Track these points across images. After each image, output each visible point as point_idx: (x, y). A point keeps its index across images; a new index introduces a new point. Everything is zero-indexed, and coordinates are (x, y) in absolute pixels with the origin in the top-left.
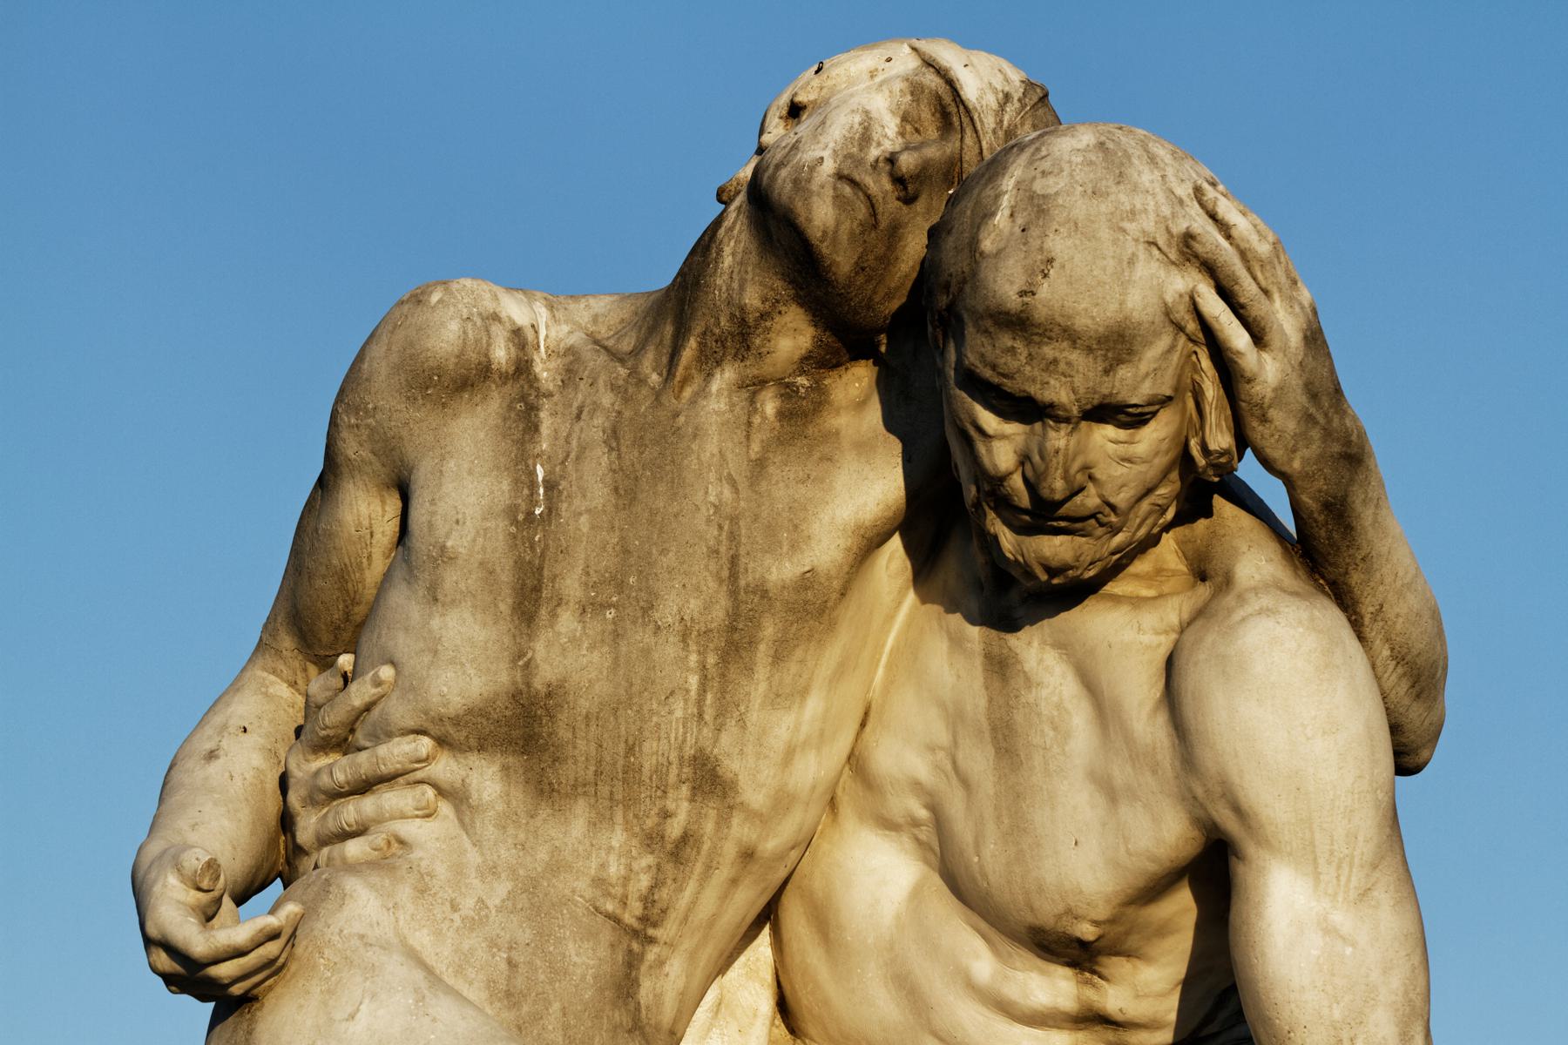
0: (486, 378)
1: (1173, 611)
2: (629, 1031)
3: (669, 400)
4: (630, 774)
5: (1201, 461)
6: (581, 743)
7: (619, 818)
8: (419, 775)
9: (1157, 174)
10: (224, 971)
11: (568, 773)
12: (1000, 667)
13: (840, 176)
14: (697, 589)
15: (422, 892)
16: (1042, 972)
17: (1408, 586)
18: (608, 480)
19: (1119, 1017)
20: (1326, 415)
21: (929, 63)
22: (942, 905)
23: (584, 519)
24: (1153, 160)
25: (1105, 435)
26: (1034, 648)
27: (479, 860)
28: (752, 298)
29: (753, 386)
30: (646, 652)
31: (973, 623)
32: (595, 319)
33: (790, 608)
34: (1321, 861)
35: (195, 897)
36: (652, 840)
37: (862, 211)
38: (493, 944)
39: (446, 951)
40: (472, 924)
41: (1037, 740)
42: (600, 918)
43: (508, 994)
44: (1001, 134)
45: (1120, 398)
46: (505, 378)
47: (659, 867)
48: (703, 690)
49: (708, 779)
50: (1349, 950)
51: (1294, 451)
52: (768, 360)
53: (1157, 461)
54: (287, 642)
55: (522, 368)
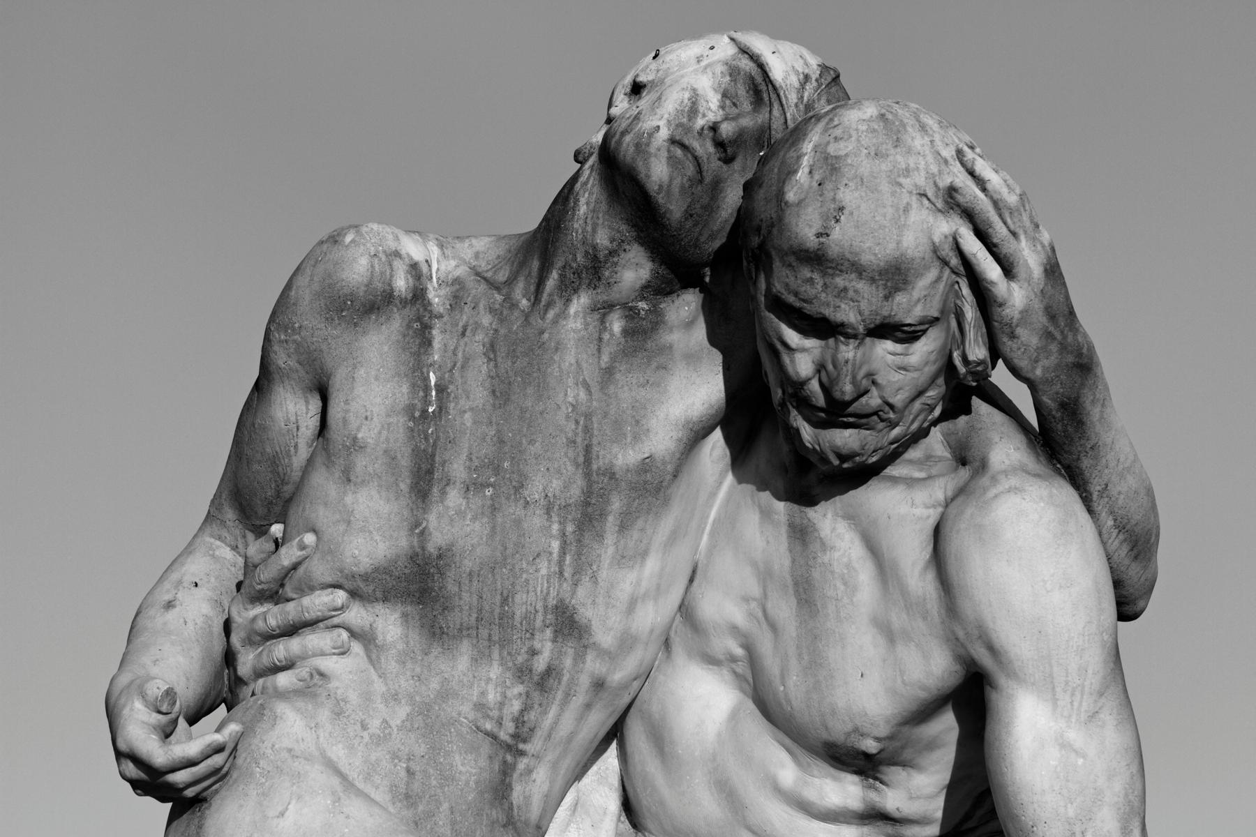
0: (389, 302)
1: (939, 490)
2: (504, 826)
3: (536, 321)
4: (505, 619)
5: (962, 370)
6: (465, 595)
7: (496, 655)
8: (336, 621)
9: (927, 139)
10: (180, 777)
11: (455, 619)
12: (801, 535)
13: (673, 141)
14: (559, 472)
15: (338, 714)
16: (835, 779)
17: (1128, 469)
18: (487, 385)
19: (896, 815)
20: (1062, 332)
21: (744, 51)
23: (467, 416)
24: (923, 128)
25: (885, 349)
26: (828, 519)
27: (384, 689)
28: (602, 239)
29: (603, 309)
30: (518, 522)
31: (779, 499)
32: (477, 255)
34: (1058, 690)
35: (156, 718)
36: (522, 673)
37: (690, 169)
38: (395, 756)
39: (358, 762)
40: (380, 740)
41: (830, 593)
42: (481, 735)
44: (802, 107)
45: (897, 319)
46: (404, 303)
47: (528, 695)
48: (563, 552)
49: (568, 624)
50: (1080, 761)
52: (615, 288)
53: (927, 369)
54: (230, 514)
55: (418, 295)
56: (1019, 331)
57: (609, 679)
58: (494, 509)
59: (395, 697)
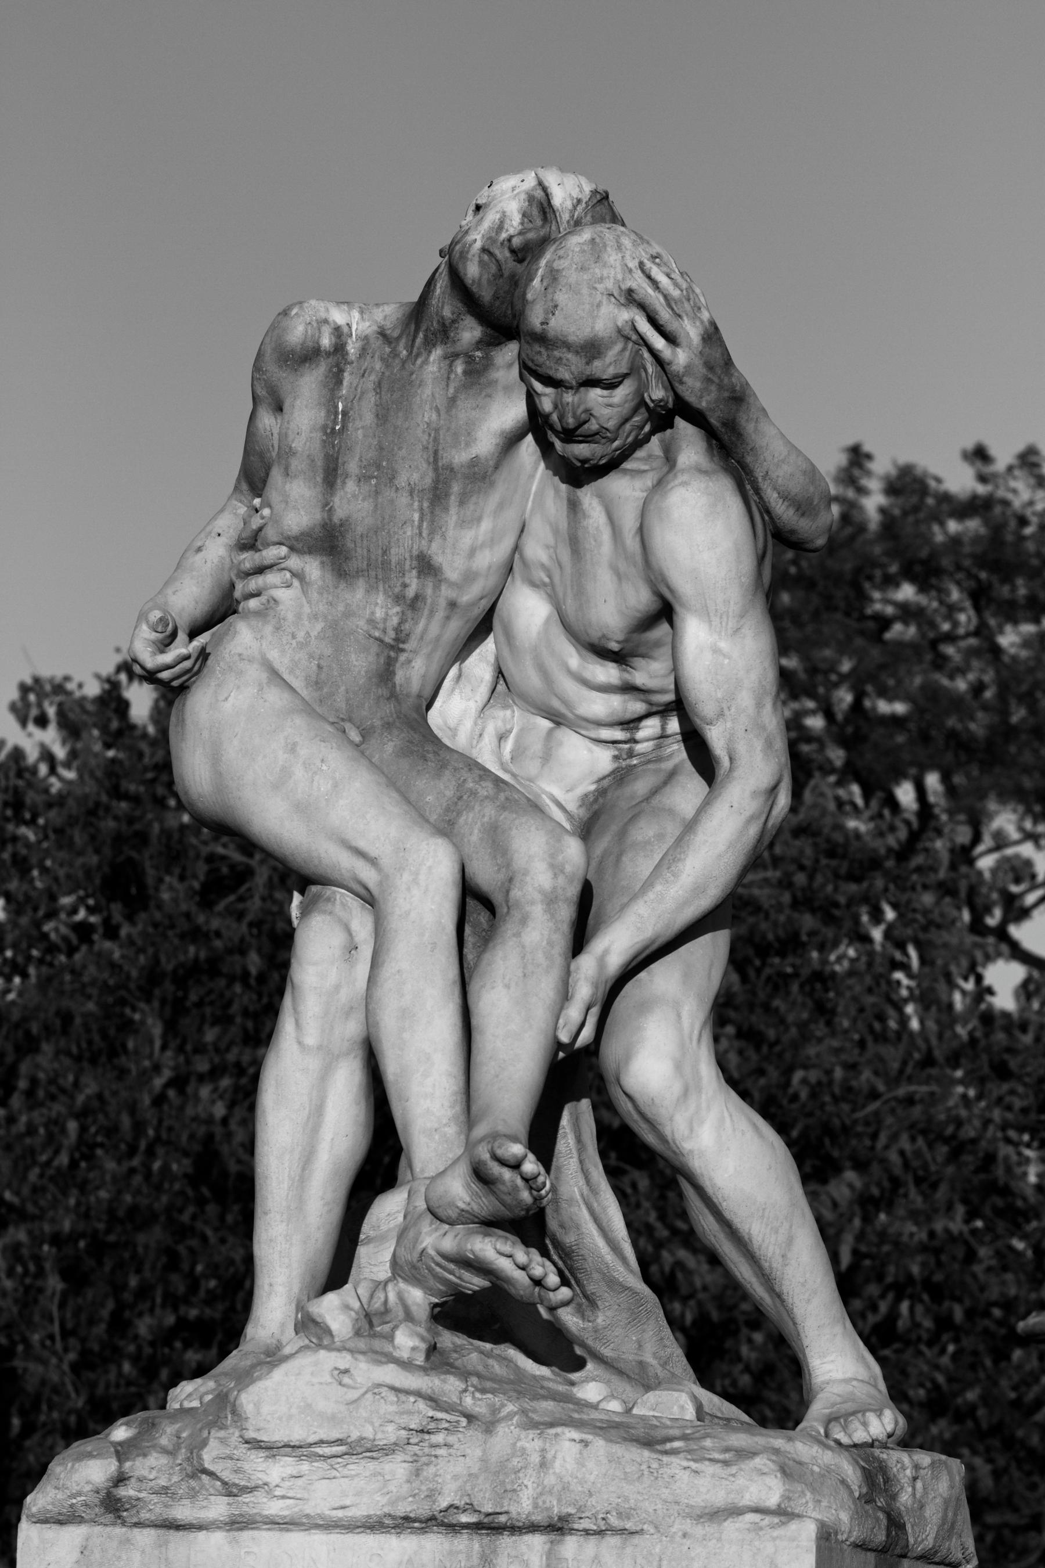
0: (318, 355)
1: (649, 481)
2: (388, 699)
3: (409, 366)
4: (386, 565)
5: (652, 405)
7: (381, 588)
8: (283, 566)
9: (620, 255)
10: (165, 675)
11: (353, 565)
12: (574, 506)
13: (484, 250)
14: (417, 467)
15: (278, 629)
16: (602, 665)
17: (783, 461)
19: (643, 688)
20: (719, 377)
21: (540, 184)
22: (557, 630)
23: (360, 432)
24: (619, 247)
25: (595, 395)
26: (587, 496)
27: (309, 611)
28: (447, 312)
29: (451, 358)
30: (392, 502)
31: (563, 482)
32: (385, 317)
33: (466, 477)
35: (154, 636)
36: (399, 599)
37: (493, 268)
38: (311, 656)
39: (286, 661)
40: (302, 646)
41: (587, 546)
43: (317, 683)
44: (572, 223)
45: (597, 376)
46: (328, 354)
47: (403, 613)
48: (421, 520)
49: (426, 567)
50: (726, 661)
51: (701, 397)
52: (458, 344)
53: (627, 405)
54: (244, 487)
55: (339, 348)
56: (685, 379)
57: (459, 600)
58: (377, 493)
59: (315, 617)
